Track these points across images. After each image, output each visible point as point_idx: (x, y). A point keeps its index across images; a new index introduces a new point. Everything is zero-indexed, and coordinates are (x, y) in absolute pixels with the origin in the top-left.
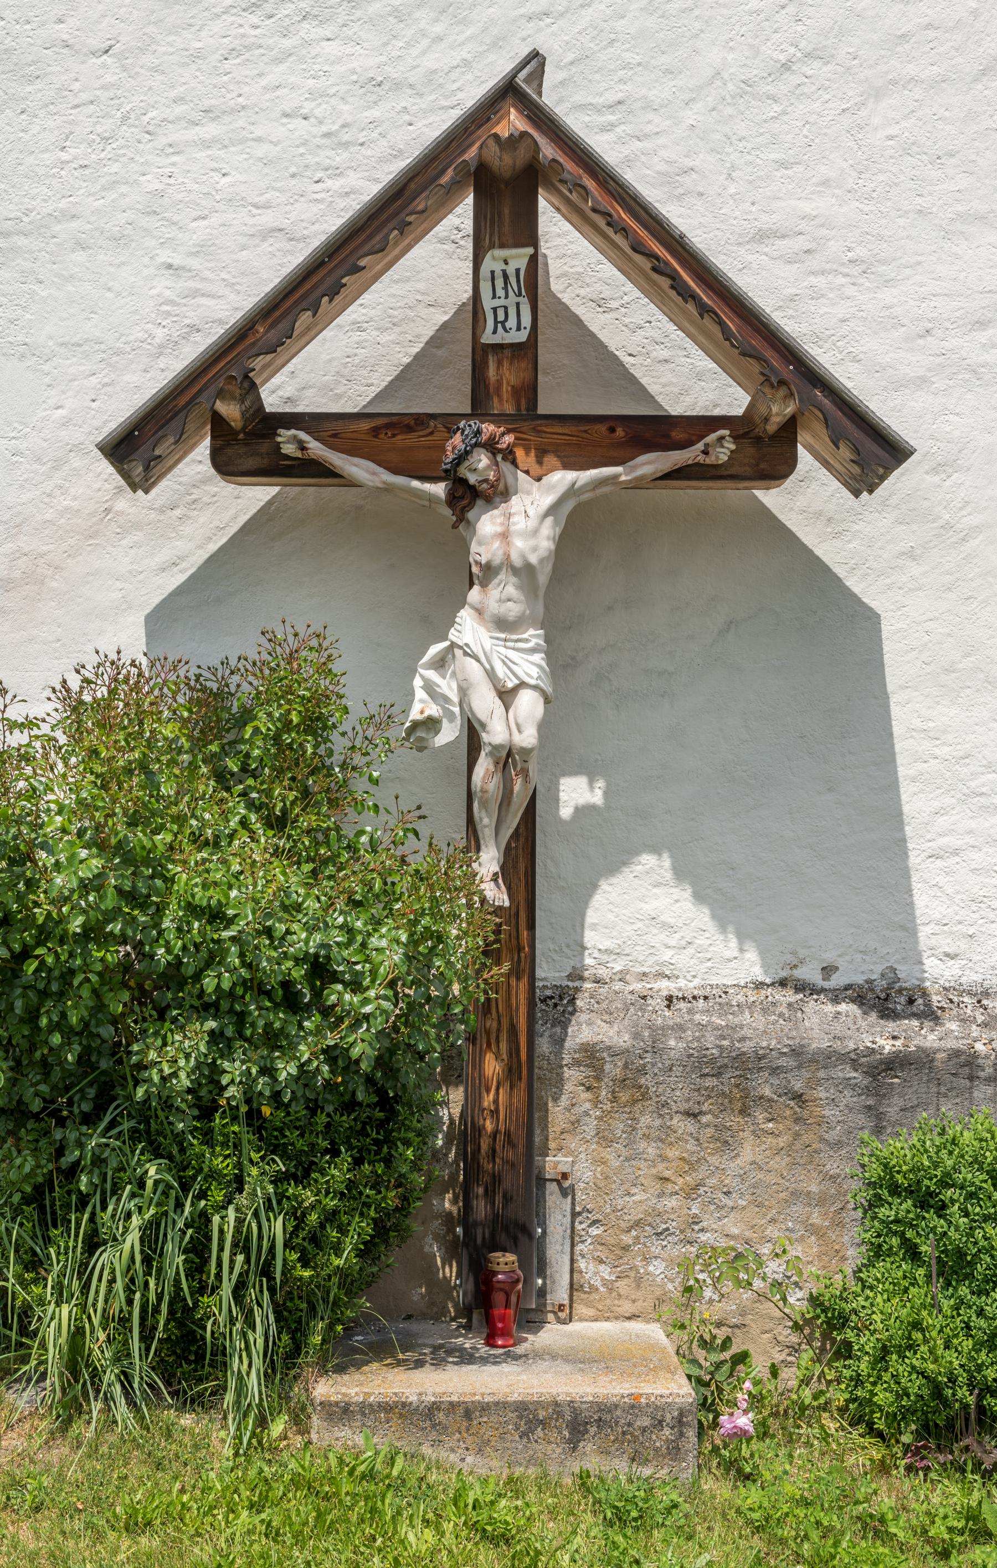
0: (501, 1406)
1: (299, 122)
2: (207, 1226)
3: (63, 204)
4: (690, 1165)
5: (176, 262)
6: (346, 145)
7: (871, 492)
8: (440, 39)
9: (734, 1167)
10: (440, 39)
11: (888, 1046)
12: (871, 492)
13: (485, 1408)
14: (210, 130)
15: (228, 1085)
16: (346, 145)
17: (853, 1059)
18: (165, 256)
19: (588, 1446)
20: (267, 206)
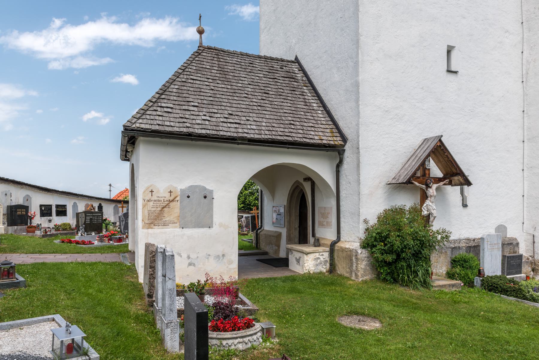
0: (447, 284)
1: (396, 136)
2: (71, 276)
3: (372, 145)
4: (437, 259)
5: (385, 153)
6: (401, 139)
7: (122, 132)
8: (410, 126)
9: (441, 259)
10: (410, 126)
11: (453, 246)
12: (122, 132)
13: (446, 285)
14: (387, 136)
15: (288, 254)
16: (401, 139)
17: (450, 248)
18: (383, 153)
19: (454, 288)
20: (393, 147)
